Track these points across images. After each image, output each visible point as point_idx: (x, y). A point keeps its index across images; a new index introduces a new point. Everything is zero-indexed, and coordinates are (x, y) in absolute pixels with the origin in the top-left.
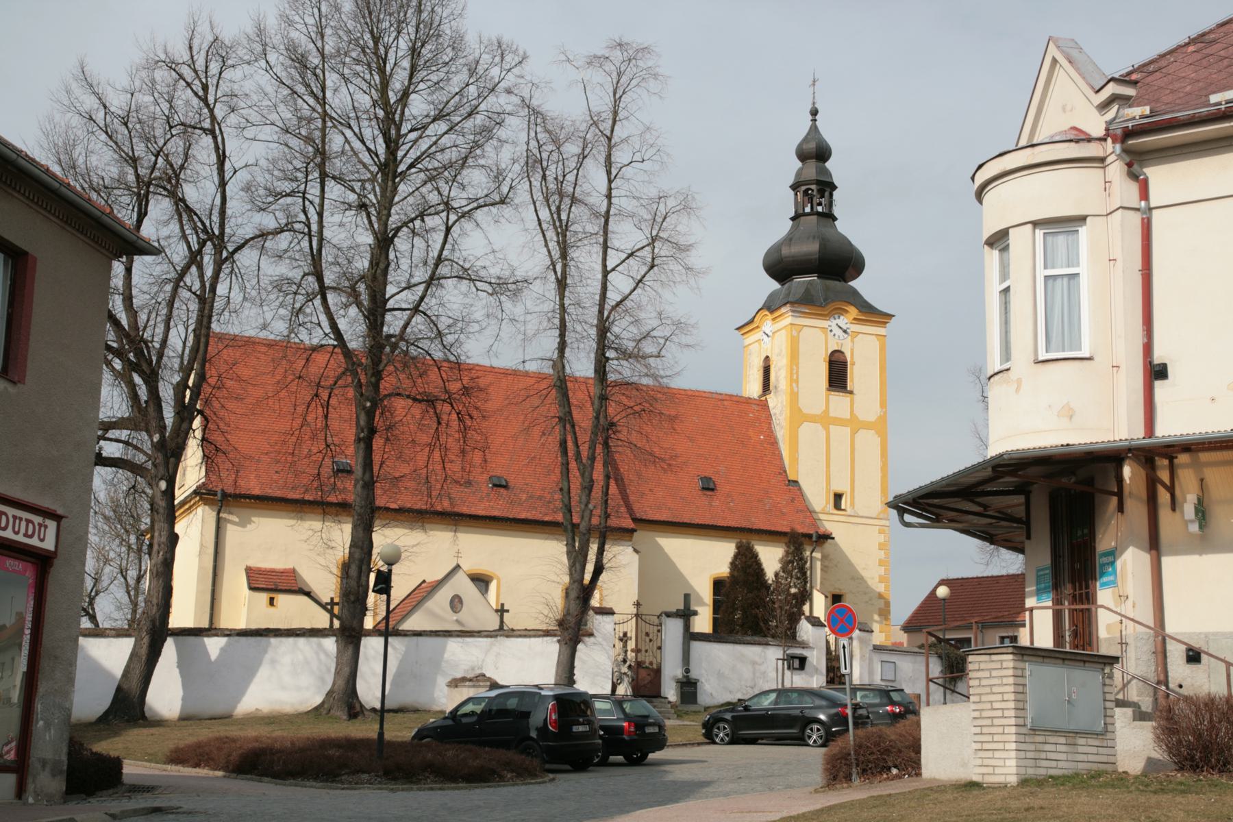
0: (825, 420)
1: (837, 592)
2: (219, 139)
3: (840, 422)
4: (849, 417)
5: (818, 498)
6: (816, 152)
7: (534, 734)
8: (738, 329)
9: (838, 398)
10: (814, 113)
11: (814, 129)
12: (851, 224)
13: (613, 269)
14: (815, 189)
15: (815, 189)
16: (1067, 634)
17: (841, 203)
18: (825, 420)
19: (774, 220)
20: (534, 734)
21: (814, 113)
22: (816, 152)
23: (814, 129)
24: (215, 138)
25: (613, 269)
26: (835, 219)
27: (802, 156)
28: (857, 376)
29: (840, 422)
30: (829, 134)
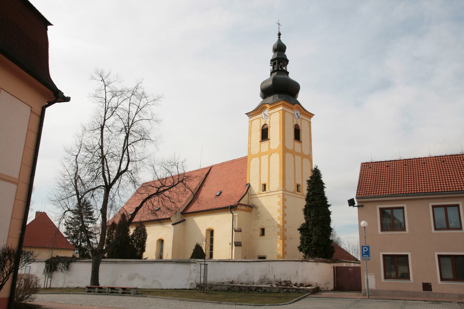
0: (293, 153)
1: (262, 227)
2: (202, 275)
3: (298, 154)
4: (304, 159)
5: (256, 188)
6: (280, 48)
7: (275, 286)
9: (297, 144)
10: (279, 34)
11: (279, 40)
12: (294, 72)
13: (130, 144)
14: (280, 60)
15: (280, 60)
16: (344, 265)
17: (289, 68)
18: (293, 153)
19: (265, 73)
20: (275, 286)
21: (279, 34)
22: (280, 48)
23: (279, 40)
25: (130, 144)
27: (275, 50)
28: (303, 135)
29: (298, 154)
30: (284, 40)
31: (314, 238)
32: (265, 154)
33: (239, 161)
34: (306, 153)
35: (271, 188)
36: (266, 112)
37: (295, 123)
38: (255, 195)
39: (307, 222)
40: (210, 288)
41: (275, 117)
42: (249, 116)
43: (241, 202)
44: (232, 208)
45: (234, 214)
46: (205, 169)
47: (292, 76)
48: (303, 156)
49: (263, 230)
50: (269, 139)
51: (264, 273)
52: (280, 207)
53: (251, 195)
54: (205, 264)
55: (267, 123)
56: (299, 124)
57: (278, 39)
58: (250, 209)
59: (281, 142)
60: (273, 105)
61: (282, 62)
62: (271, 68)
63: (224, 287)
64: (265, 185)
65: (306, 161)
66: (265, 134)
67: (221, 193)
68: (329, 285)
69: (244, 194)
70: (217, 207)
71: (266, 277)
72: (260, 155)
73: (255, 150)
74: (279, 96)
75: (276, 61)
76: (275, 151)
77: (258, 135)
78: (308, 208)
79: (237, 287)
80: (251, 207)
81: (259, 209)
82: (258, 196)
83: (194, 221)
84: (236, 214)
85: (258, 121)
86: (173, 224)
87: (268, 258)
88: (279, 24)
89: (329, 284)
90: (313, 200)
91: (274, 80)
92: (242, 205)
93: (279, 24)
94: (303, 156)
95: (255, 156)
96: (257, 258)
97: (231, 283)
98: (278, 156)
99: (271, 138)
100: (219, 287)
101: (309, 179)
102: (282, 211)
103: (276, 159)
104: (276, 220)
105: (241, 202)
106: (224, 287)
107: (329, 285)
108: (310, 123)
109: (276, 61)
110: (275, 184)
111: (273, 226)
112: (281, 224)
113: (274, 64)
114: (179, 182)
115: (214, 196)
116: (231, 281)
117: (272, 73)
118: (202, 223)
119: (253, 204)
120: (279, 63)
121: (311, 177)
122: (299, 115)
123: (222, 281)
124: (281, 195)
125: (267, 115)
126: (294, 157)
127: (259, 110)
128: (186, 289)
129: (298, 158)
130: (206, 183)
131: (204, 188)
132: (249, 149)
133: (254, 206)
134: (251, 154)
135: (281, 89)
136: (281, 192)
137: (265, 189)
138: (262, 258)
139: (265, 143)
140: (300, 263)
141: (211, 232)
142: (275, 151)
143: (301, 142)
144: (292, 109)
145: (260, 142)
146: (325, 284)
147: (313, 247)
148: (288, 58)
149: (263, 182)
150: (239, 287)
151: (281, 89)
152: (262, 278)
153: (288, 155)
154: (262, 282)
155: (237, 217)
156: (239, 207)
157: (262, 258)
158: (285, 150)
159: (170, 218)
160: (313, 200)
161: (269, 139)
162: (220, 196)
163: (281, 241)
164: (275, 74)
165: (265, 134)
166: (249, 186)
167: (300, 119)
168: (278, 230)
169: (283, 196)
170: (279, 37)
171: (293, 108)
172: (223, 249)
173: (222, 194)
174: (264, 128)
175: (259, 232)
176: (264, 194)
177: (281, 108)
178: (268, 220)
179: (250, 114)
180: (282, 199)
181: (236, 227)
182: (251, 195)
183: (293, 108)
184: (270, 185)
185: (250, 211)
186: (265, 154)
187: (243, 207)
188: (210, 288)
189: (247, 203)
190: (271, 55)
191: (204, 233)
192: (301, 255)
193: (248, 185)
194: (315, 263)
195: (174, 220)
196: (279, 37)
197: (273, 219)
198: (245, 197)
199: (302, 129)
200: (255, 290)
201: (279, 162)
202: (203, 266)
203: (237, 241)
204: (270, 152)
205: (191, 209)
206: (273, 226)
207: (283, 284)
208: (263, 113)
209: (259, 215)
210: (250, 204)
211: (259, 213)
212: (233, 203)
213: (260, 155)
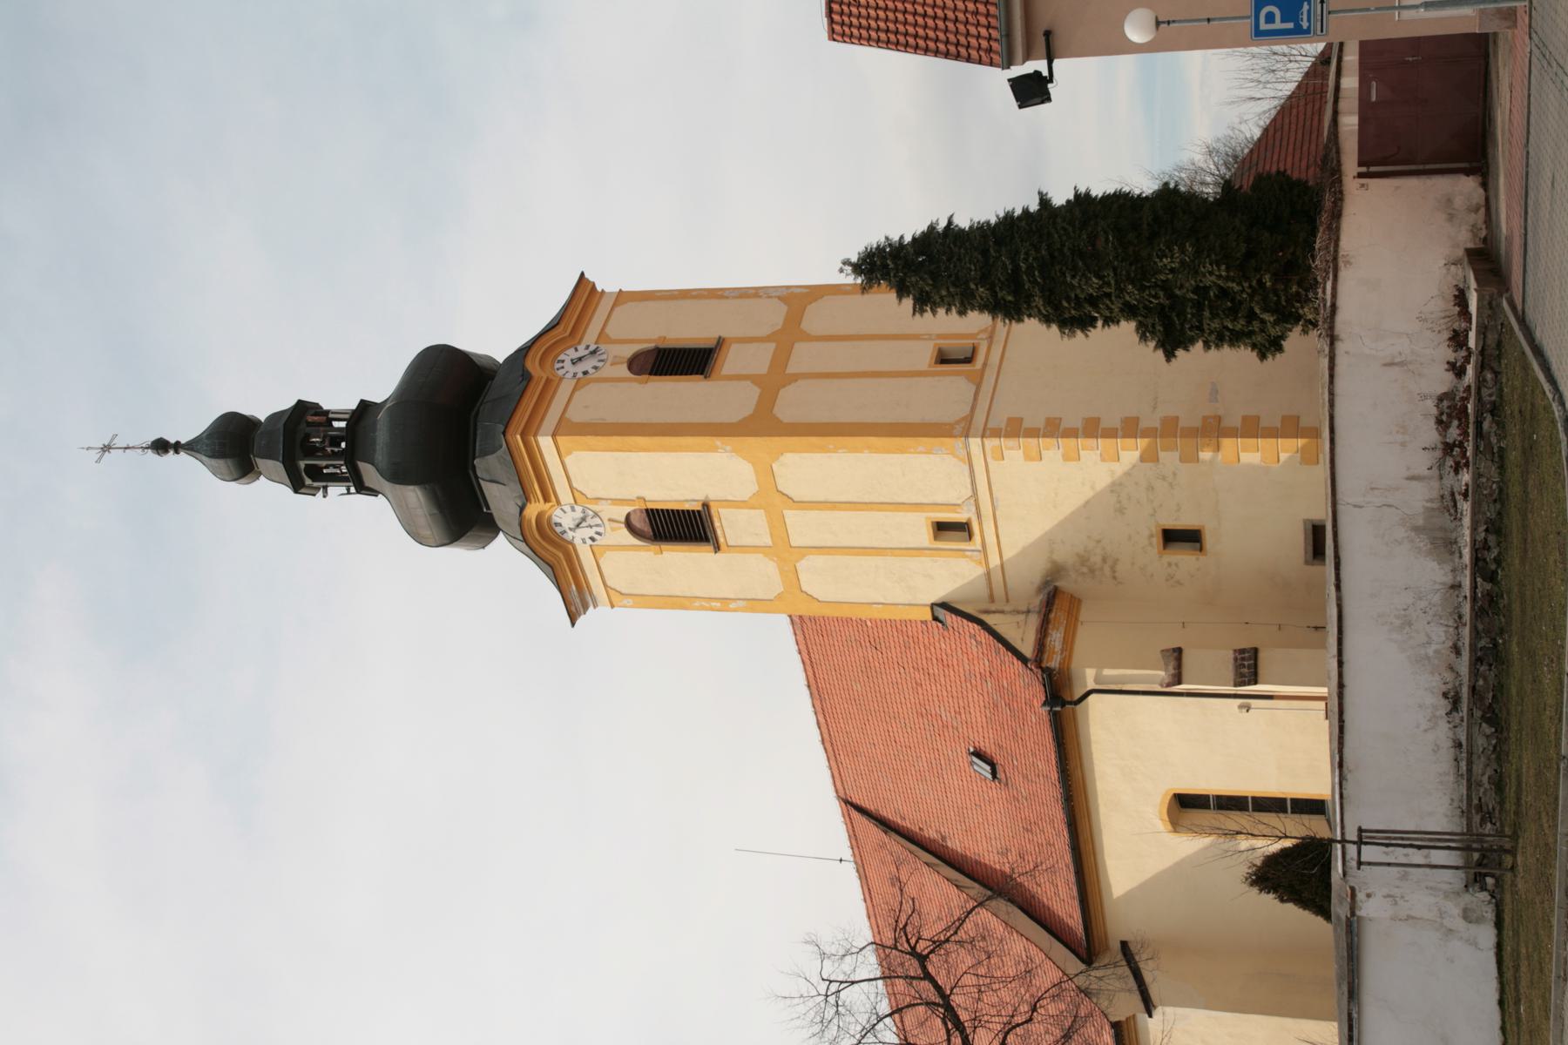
0: (773, 382)
1: (1158, 540)
3: (781, 359)
4: (805, 325)
5: (952, 575)
6: (236, 445)
7: (1466, 477)
8: (573, 624)
9: (730, 362)
10: (161, 446)
11: (191, 447)
12: (360, 373)
14: (296, 446)
15: (296, 446)
17: (339, 398)
18: (773, 382)
19: (363, 527)
20: (1466, 477)
21: (161, 446)
22: (236, 445)
23: (191, 447)
24: (1502, 468)
26: (365, 406)
28: (686, 331)
29: (781, 359)
31: (1213, 276)
32: (778, 527)
33: (815, 656)
34: (774, 316)
35: (952, 497)
36: (564, 518)
37: (623, 371)
38: (988, 574)
39: (1130, 311)
40: (1488, 816)
41: (593, 476)
42: (586, 608)
43: (1028, 649)
44: (1061, 699)
45: (1091, 685)
46: (854, 837)
47: (382, 385)
48: (789, 334)
49: (1172, 537)
50: (706, 505)
51: (1401, 533)
52: (1053, 451)
53: (992, 599)
54: (1360, 843)
55: (621, 512)
56: (629, 351)
57: (182, 454)
58: (1058, 615)
59: (718, 441)
60: (531, 481)
61: (308, 436)
62: (335, 490)
63: (1481, 742)
64: (941, 528)
65: (814, 320)
66: (680, 527)
67: (978, 754)
68: (1459, 202)
69: (984, 636)
70: (1054, 776)
71: (1420, 522)
72: (784, 552)
73: (762, 575)
74: (485, 453)
75: (302, 464)
76: (767, 475)
77: (680, 559)
78: (1058, 308)
79: (1474, 673)
80: (1055, 601)
81: (1064, 555)
82: (994, 561)
83: (1128, 896)
84: (1089, 678)
85: (610, 562)
86: (1149, 1008)
87: (1321, 513)
88: (106, 448)
89: (1449, 201)
90: (1014, 282)
91: (399, 475)
92: (1043, 640)
93: (106, 448)
94: (789, 334)
95: (791, 577)
96: (1315, 569)
97: (1455, 703)
98: (789, 458)
99: (702, 497)
100: (1478, 768)
101: (908, 302)
102: (1072, 441)
103: (807, 469)
104: (1119, 469)
105: (1028, 649)
106: (1481, 742)
107: (1459, 202)
108: (622, 297)
109: (302, 464)
110: (933, 475)
111: (1151, 488)
112: (1142, 443)
113: (316, 473)
114: (928, 976)
115: (995, 791)
116: (1445, 705)
117: (362, 488)
118: (1139, 852)
119: (1039, 590)
120: (311, 451)
121: (902, 291)
122: (582, 352)
123: (1447, 754)
124: (991, 443)
125: (578, 514)
126: (796, 377)
127: (552, 553)
128: (1499, 947)
129: (803, 357)
130: (931, 833)
131: (956, 844)
132: (755, 605)
133: (1046, 583)
134: (779, 597)
135: (446, 441)
136: (975, 443)
137: (963, 528)
138: (1318, 541)
139: (727, 523)
140: (1341, 347)
141: (1186, 804)
142: (767, 475)
143: (721, 342)
144: (550, 385)
145: (717, 548)
146: (1451, 217)
147: (1260, 282)
148: (287, 403)
149: (925, 536)
150: (1476, 661)
151: (446, 441)
152: (1423, 543)
153: (789, 406)
154: (1449, 546)
155: (1107, 672)
156: (1054, 663)
157: (1318, 541)
158: (763, 423)
159: (1117, 1027)
160: (1014, 282)
161: (706, 505)
162: (998, 759)
163: (1227, 443)
164: (368, 472)
165: (680, 527)
166: (944, 605)
167: (603, 347)
168: (1169, 459)
169: (996, 433)
170: (177, 447)
171: (548, 381)
172: (1273, 745)
173: (988, 748)
174: (647, 529)
175: (1183, 558)
176: (985, 531)
177: (545, 443)
178: (1121, 510)
179: (576, 603)
180: (1012, 442)
181: (1158, 675)
182: (992, 599)
183: (548, 381)
184: (940, 499)
185: (1075, 603)
186: (778, 527)
187: (1056, 638)
188: (1488, 816)
189: (1034, 621)
190: (269, 492)
191: (1188, 845)
192: (1297, 342)
193: (941, 613)
194: (1344, 274)
195: (1125, 1004)
196: (177, 447)
197: (1115, 487)
198: (1000, 630)
199: (655, 337)
200: (1491, 578)
201: (818, 457)
202: (1369, 853)
203: (1229, 671)
204: (772, 500)
205: (1066, 908)
206: (1151, 488)
207: (1454, 433)
208: (570, 535)
209: (1096, 559)
210: (1037, 601)
211: (1083, 560)
212: (1031, 691)
213: (784, 552)
